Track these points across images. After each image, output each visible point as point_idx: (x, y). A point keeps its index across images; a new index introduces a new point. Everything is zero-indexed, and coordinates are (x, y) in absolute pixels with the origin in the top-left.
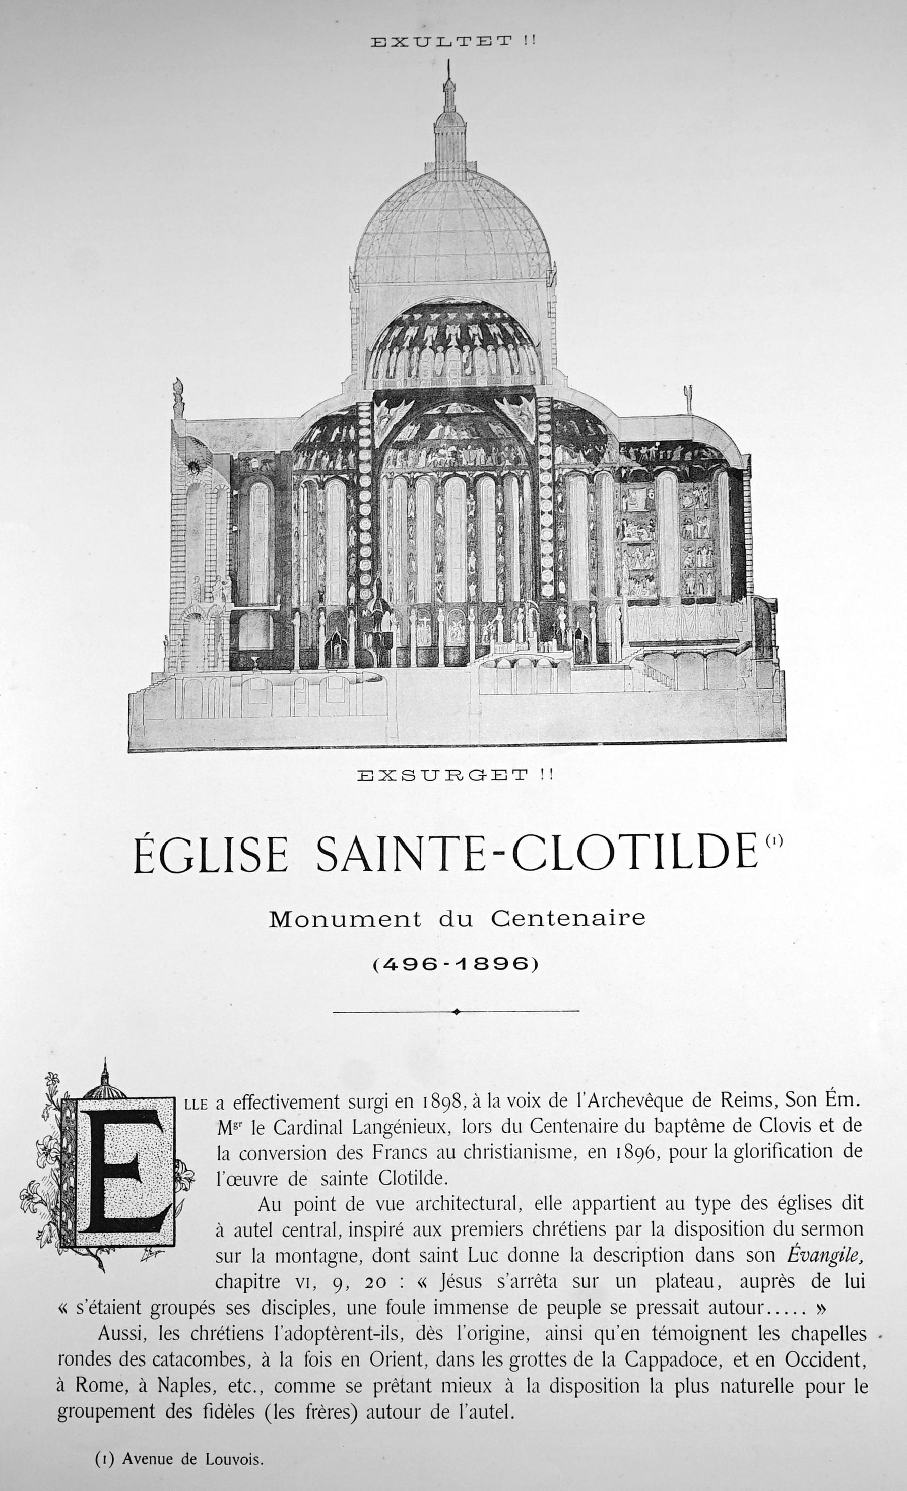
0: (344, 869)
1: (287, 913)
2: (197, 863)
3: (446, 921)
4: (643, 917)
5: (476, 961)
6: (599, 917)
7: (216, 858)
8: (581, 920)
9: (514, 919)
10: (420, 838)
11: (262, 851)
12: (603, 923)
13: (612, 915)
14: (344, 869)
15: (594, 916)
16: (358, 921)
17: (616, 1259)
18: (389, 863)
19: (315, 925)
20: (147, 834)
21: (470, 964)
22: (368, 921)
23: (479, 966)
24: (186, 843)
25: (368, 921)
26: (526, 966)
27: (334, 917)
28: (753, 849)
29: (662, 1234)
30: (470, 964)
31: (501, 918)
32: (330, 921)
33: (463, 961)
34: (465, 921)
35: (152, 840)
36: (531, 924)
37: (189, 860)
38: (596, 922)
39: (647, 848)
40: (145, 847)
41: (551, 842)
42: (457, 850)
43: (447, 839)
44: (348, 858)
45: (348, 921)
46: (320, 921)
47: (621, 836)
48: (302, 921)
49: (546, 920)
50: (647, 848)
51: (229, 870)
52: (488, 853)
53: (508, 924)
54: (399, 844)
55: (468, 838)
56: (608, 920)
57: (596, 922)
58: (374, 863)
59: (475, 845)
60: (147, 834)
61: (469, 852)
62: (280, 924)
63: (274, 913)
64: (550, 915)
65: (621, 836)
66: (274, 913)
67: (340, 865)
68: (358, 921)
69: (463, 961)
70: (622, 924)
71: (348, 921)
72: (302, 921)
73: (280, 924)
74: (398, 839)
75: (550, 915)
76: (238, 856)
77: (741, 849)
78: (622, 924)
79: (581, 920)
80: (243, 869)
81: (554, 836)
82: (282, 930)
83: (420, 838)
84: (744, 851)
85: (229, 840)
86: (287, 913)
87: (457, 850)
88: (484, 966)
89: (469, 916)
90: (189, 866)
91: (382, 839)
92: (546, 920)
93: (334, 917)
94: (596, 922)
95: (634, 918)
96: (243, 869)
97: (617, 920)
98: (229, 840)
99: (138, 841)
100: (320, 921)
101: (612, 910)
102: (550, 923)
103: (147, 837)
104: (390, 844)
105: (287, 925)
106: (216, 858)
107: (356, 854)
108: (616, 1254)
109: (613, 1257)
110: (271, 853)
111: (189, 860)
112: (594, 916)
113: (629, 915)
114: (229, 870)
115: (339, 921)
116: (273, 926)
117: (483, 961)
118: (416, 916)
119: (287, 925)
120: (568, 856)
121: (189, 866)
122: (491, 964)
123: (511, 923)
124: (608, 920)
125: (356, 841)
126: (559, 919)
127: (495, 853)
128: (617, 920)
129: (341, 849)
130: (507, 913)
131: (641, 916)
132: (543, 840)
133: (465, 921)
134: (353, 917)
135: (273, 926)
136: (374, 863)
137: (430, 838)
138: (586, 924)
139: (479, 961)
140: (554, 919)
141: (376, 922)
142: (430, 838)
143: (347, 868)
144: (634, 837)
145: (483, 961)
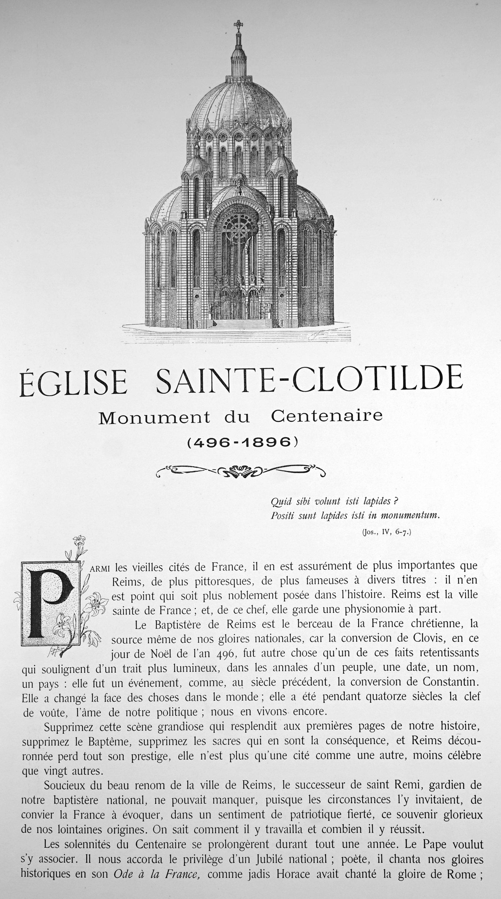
0: (176, 392)
1: (112, 413)
2: (63, 389)
3: (230, 418)
4: (381, 415)
5: (254, 440)
6: (349, 415)
7: (77, 384)
8: (336, 417)
9: (288, 417)
10: (229, 370)
11: (109, 380)
12: (352, 419)
13: (359, 414)
14: (176, 392)
15: (346, 415)
16: (164, 419)
17: (227, 583)
18: (207, 387)
19: (133, 423)
20: (28, 370)
21: (251, 442)
22: (171, 419)
23: (256, 444)
24: (55, 375)
25: (171, 419)
26: (289, 443)
27: (146, 416)
28: (460, 376)
29: (358, 583)
30: (251, 442)
31: (278, 416)
32: (143, 419)
33: (247, 440)
34: (243, 418)
35: (32, 373)
36: (300, 421)
37: (58, 386)
38: (347, 419)
39: (384, 376)
40: (27, 379)
41: (318, 371)
42: (254, 379)
43: (247, 370)
44: (179, 384)
45: (157, 419)
46: (136, 419)
47: (366, 367)
48: (123, 420)
49: (311, 417)
50: (384, 376)
51: (87, 393)
52: (277, 379)
53: (283, 420)
54: (213, 373)
55: (263, 370)
56: (355, 417)
57: (347, 419)
58: (197, 387)
59: (268, 374)
60: (28, 370)
61: (263, 379)
62: (107, 422)
63: (102, 414)
64: (314, 413)
65: (366, 367)
66: (102, 414)
67: (173, 389)
68: (164, 419)
69: (247, 440)
70: (365, 420)
71: (157, 419)
72: (123, 420)
73: (107, 422)
74: (213, 370)
75: (314, 413)
76: (93, 384)
77: (450, 376)
78: (365, 420)
79: (336, 417)
80: (95, 392)
81: (320, 368)
82: (109, 425)
83: (229, 370)
84: (452, 377)
85: (86, 372)
86: (112, 413)
87: (254, 379)
88: (260, 444)
89: (247, 415)
90: (58, 391)
91: (202, 370)
92: (311, 417)
93: (146, 416)
94: (347, 419)
95: (374, 416)
96: (95, 392)
97: (362, 417)
98: (86, 372)
99: (22, 375)
100: (136, 419)
101: (359, 410)
102: (314, 420)
103: (28, 372)
104: (207, 374)
105: (112, 423)
106: (77, 384)
107: (184, 381)
108: (227, 581)
109: (226, 583)
110: (115, 381)
111: (58, 386)
112: (346, 415)
113: (370, 414)
114: (87, 393)
115: (150, 419)
116: (102, 423)
117: (260, 440)
118: (206, 415)
119: (112, 423)
120: (330, 381)
121: (58, 391)
122: (265, 442)
123: (286, 419)
124: (355, 417)
125: (184, 372)
126: (320, 417)
127: (281, 380)
128: (362, 417)
129: (174, 379)
130: (283, 412)
131: (379, 414)
132: (313, 370)
133: (243, 418)
134: (160, 416)
135: (102, 423)
136: (197, 387)
137: (235, 369)
138: (340, 420)
139: (257, 440)
140: (317, 417)
141: (178, 420)
142: (235, 369)
143: (178, 391)
144: (376, 368)
145: (260, 440)
